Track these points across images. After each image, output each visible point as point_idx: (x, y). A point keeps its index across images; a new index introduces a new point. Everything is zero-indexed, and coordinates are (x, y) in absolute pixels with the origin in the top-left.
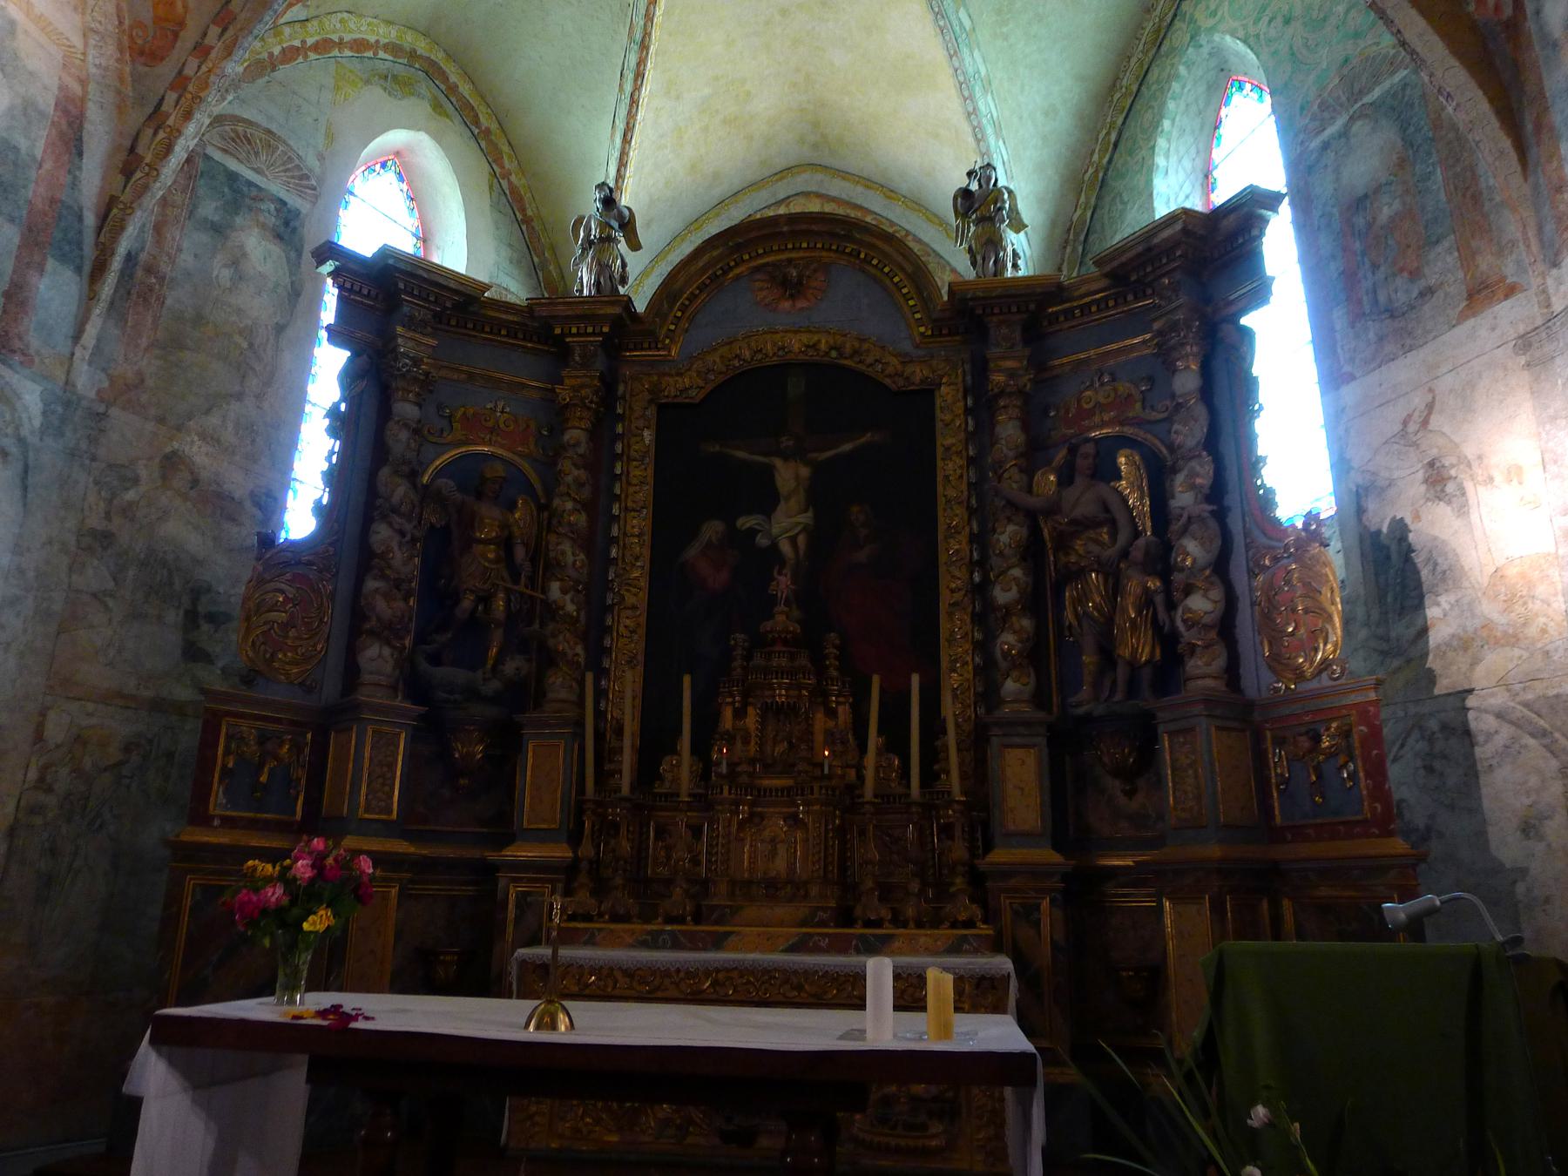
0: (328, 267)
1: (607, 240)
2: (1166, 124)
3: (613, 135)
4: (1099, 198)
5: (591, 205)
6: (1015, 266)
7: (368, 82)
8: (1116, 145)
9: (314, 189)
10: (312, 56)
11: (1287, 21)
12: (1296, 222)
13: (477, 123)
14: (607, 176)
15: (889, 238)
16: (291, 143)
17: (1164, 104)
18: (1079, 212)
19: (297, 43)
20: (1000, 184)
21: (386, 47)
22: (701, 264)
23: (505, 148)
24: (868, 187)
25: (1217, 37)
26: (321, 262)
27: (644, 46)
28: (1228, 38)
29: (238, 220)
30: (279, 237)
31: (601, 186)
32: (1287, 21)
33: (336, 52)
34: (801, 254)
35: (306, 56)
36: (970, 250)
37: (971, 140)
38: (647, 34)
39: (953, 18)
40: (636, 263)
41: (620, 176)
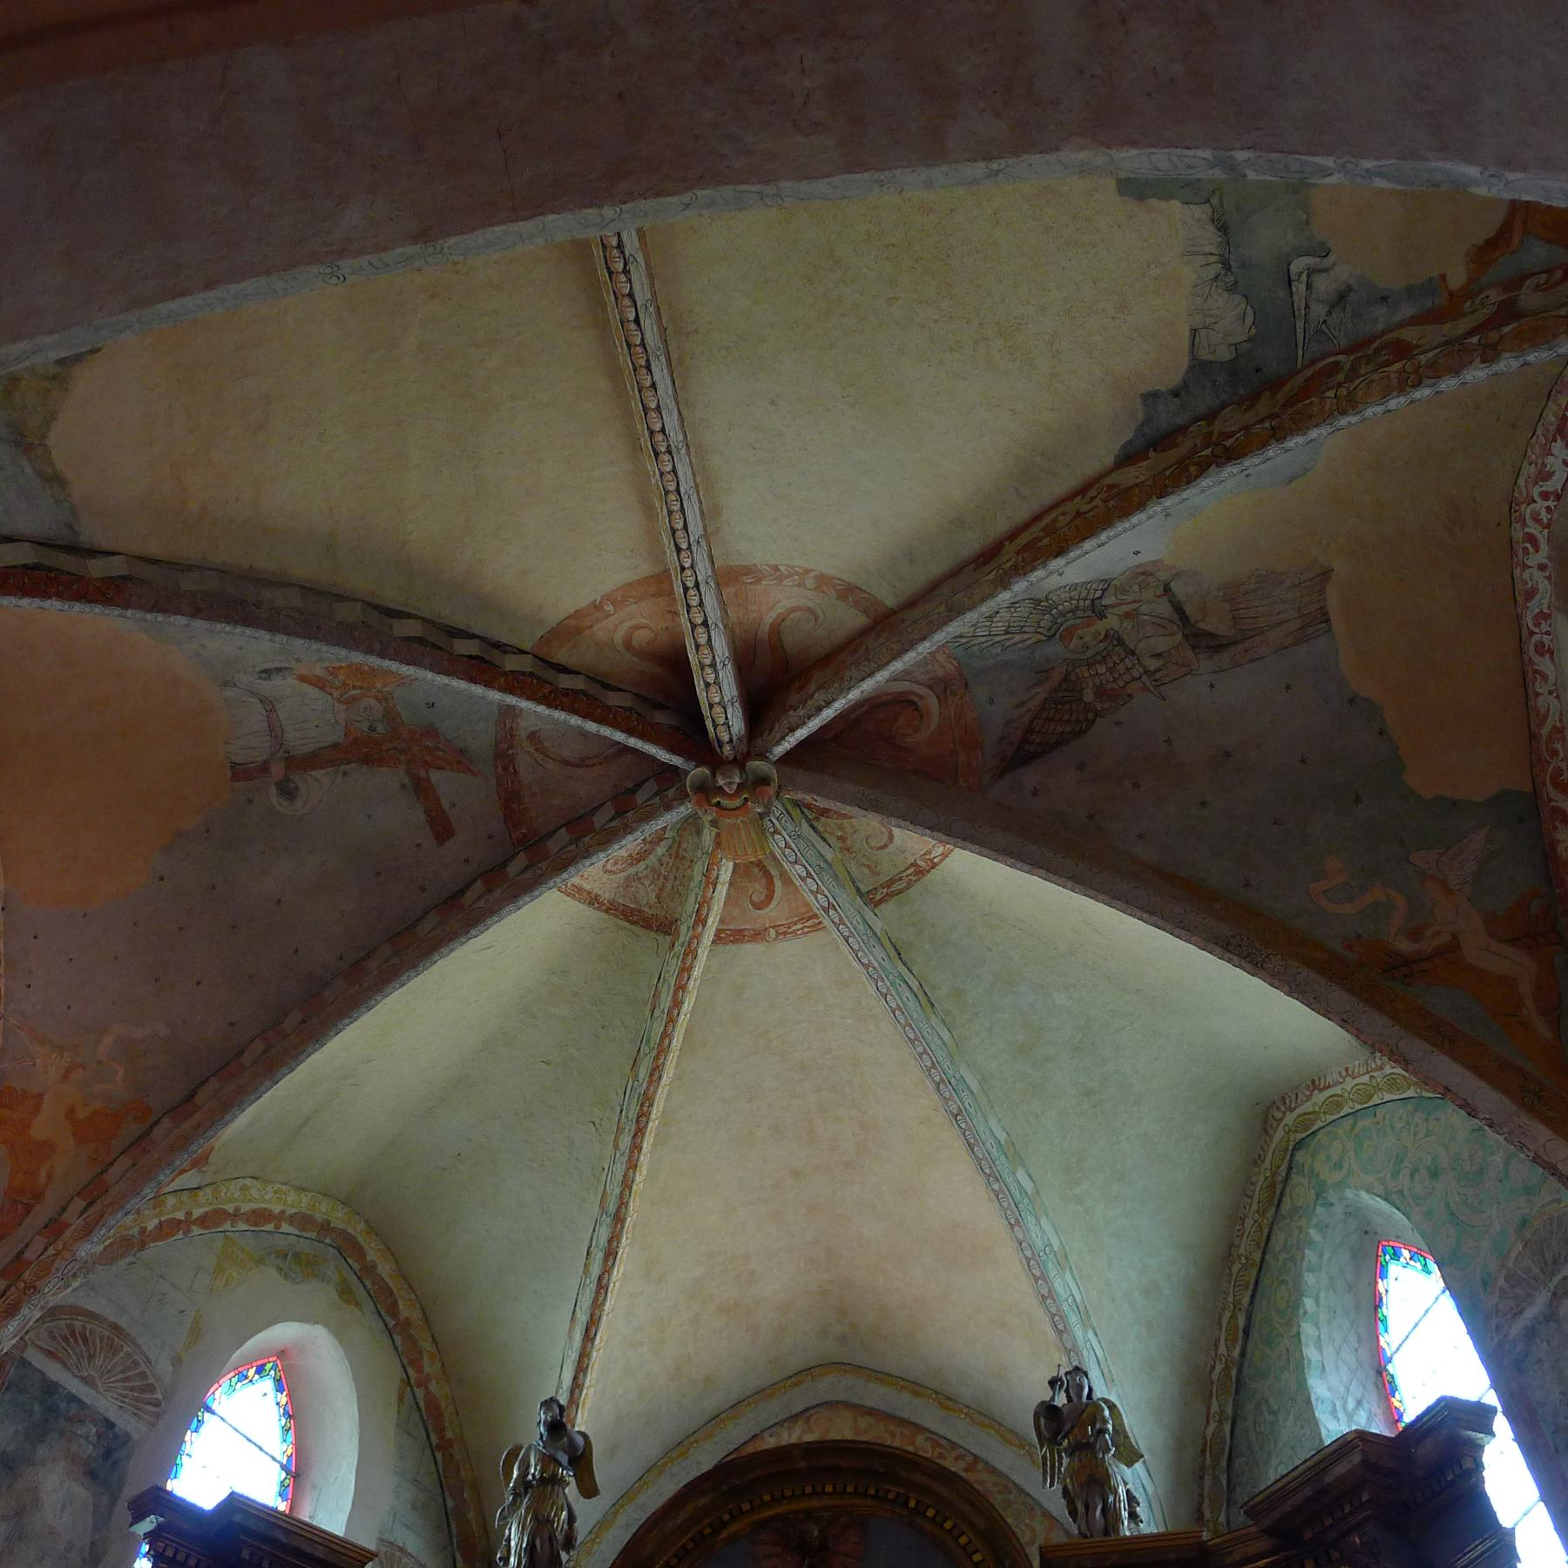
0: (148, 1525)
1: (551, 1481)
2: (1308, 1303)
3: (571, 1330)
4: (1236, 1404)
5: (533, 1430)
6: (1133, 1516)
7: (260, 1262)
8: (1246, 1332)
9: (157, 1405)
10: (196, 1230)
11: (1434, 1174)
12: (1519, 1439)
13: (394, 1311)
14: (559, 1386)
15: (949, 1477)
16: (141, 1342)
17: (1298, 1279)
18: (1213, 1426)
19: (180, 1215)
20: (1097, 1394)
21: (292, 1220)
22: (680, 1520)
23: (427, 1345)
24: (917, 1394)
25: (1349, 1193)
26: (138, 1518)
27: (619, 1219)
28: (1363, 1194)
29: (42, 1451)
30: (92, 1474)
31: (549, 1404)
32: (1434, 1174)
33: (227, 1226)
34: (827, 1502)
35: (187, 1232)
36: (1066, 1493)
37: (1050, 1331)
38: (623, 1204)
39: (1009, 1180)
40: (587, 1512)
41: (576, 1385)
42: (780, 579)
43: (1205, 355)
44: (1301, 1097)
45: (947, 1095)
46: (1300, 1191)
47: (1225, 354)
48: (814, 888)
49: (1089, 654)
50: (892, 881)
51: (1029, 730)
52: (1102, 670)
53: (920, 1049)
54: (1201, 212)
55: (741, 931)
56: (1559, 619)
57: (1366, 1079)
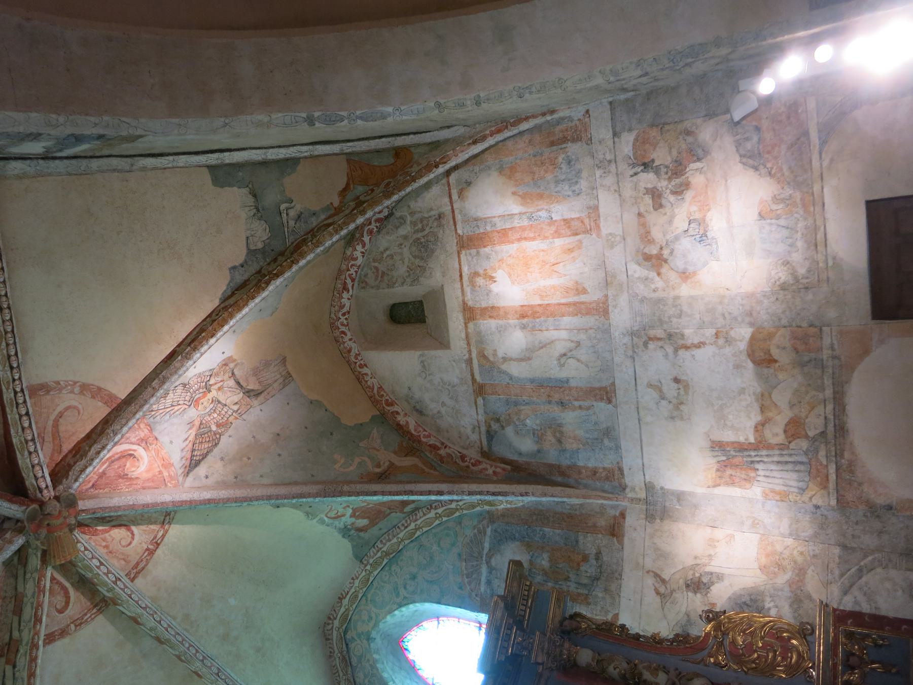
42: (60, 390)
43: (252, 247)
44: (337, 609)
45: (209, 665)
46: (357, 647)
47: (260, 245)
48: (106, 571)
49: (208, 410)
50: (138, 564)
51: (193, 450)
52: (215, 415)
53: (187, 645)
54: (245, 191)
55: (54, 632)
56: (363, 353)
57: (364, 574)
